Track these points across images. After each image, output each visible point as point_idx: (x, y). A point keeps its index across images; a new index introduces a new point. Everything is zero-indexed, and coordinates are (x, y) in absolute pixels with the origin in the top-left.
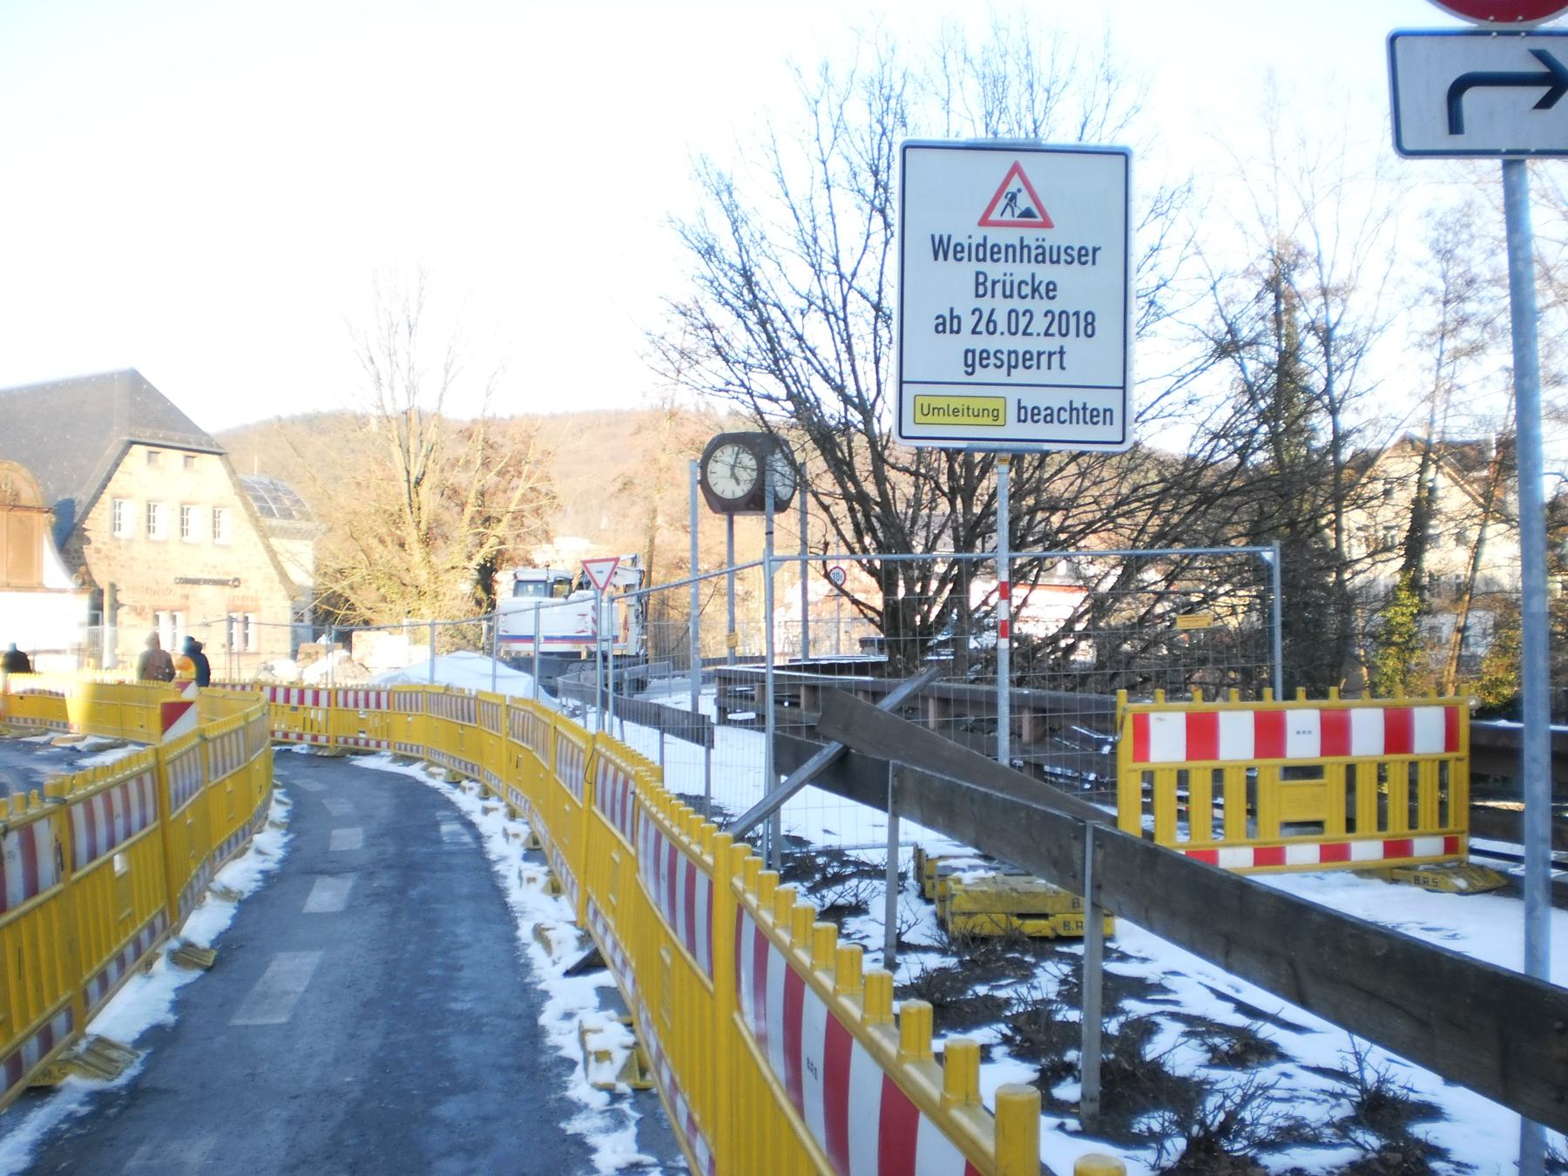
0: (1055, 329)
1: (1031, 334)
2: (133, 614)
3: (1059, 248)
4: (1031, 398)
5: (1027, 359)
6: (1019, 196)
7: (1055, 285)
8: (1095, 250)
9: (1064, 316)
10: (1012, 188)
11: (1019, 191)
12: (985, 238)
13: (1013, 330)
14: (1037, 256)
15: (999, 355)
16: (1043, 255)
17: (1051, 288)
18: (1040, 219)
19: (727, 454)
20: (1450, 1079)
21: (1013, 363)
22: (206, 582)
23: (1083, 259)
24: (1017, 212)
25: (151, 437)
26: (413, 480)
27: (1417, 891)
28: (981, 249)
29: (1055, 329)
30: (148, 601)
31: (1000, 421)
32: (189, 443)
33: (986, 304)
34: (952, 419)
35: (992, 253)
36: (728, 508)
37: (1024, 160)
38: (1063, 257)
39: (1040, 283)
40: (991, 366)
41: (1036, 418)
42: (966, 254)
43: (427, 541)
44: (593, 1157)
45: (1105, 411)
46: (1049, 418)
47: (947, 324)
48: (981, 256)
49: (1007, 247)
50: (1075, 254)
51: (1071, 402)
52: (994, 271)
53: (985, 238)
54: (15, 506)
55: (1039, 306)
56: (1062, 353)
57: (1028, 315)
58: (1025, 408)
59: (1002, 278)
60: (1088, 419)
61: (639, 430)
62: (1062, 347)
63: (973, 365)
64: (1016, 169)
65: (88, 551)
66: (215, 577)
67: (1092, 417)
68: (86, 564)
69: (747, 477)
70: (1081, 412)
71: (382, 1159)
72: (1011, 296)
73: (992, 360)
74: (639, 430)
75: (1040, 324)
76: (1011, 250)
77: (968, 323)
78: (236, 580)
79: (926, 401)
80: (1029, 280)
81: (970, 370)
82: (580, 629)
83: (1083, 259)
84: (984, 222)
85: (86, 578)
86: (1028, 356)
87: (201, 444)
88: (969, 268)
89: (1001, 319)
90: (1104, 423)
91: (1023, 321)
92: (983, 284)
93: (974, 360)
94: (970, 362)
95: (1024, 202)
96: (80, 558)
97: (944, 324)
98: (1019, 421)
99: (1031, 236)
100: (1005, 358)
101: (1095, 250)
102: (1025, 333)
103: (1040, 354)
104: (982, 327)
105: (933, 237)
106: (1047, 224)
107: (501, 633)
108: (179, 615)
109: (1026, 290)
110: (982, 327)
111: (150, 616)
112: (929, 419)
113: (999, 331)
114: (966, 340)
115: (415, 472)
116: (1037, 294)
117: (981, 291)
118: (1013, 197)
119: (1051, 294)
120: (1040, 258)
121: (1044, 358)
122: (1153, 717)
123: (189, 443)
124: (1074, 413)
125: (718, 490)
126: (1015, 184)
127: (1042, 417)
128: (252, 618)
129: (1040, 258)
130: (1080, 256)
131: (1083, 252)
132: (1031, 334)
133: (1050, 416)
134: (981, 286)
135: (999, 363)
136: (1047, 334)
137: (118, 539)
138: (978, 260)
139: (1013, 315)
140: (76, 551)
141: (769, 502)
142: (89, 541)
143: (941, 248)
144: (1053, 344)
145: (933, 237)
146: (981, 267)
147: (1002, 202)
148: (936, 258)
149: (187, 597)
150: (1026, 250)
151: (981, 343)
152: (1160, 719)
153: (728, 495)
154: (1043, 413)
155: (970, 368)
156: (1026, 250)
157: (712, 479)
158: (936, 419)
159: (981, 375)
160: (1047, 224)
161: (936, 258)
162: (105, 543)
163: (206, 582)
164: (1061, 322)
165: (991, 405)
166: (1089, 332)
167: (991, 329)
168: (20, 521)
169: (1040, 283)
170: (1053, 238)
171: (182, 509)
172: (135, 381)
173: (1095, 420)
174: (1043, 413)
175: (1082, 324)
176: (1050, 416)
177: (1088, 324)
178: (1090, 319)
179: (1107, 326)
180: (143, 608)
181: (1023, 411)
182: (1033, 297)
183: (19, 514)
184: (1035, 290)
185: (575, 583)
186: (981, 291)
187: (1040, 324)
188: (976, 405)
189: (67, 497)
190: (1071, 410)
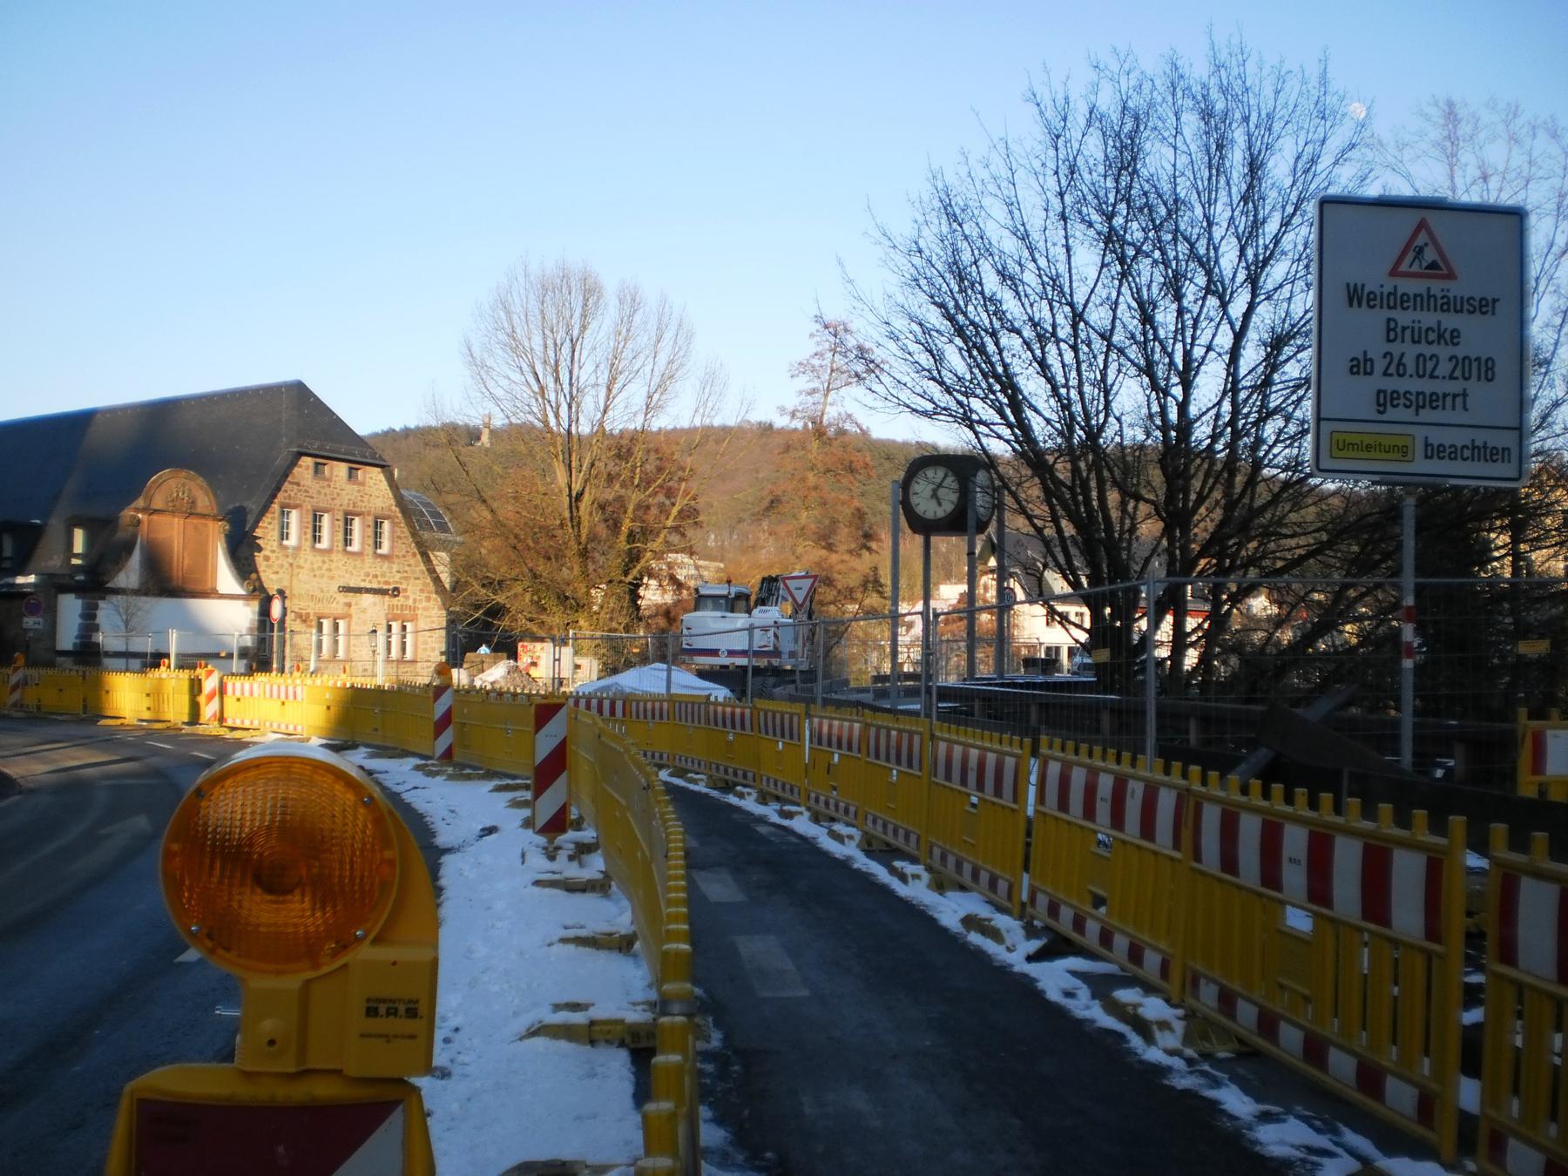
0: (1458, 373)
1: (1437, 377)
2: (298, 621)
4: (1438, 437)
5: (1434, 401)
6: (1427, 250)
7: (1459, 333)
8: (1495, 301)
9: (1467, 362)
10: (1420, 241)
11: (1426, 244)
13: (1421, 373)
14: (1443, 304)
16: (1448, 305)
17: (1455, 336)
18: (1445, 271)
19: (936, 474)
21: (1421, 404)
22: (368, 591)
23: (1484, 309)
24: (1425, 264)
25: (319, 448)
26: (574, 494)
27: (606, 952)
29: (1458, 373)
30: (312, 609)
31: (1409, 457)
32: (354, 455)
33: (1396, 348)
34: (1365, 455)
36: (925, 527)
37: (1432, 218)
38: (1466, 307)
39: (1446, 330)
40: (1401, 407)
41: (1441, 455)
42: (1378, 302)
43: (584, 554)
45: (1503, 449)
46: (1453, 455)
47: (1360, 366)
48: (1392, 304)
49: (1415, 296)
50: (1476, 304)
51: (1365, 353)
52: (1404, 318)
54: (191, 514)
55: (1444, 352)
56: (1465, 395)
57: (1434, 359)
58: (1432, 445)
59: (1411, 325)
60: (1488, 457)
61: (788, 448)
62: (1465, 390)
63: (1384, 405)
64: (1422, 225)
65: (259, 558)
66: (375, 586)
67: (1492, 455)
68: (257, 572)
69: (949, 499)
70: (1482, 450)
72: (1419, 342)
73: (1402, 401)
74: (788, 448)
75: (1444, 368)
77: (1380, 365)
78: (396, 589)
79: (1342, 437)
80: (1435, 327)
81: (1382, 409)
82: (763, 644)
84: (1394, 272)
85: (257, 584)
86: (1434, 398)
87: (366, 457)
88: (1380, 315)
89: (1409, 361)
90: (1503, 461)
91: (1430, 365)
92: (1394, 330)
93: (1385, 400)
95: (1430, 255)
96: (250, 565)
97: (1358, 366)
98: (1426, 457)
99: (1436, 287)
100: (1413, 398)
101: (1495, 301)
102: (1432, 376)
103: (1445, 395)
104: (1392, 370)
105: (1348, 285)
106: (1451, 276)
107: (685, 646)
108: (341, 623)
109: (1432, 336)
110: (1392, 370)
111: (314, 623)
112: (1344, 454)
113: (1408, 374)
114: (1378, 381)
115: (576, 487)
116: (1442, 341)
117: (1392, 337)
118: (1420, 251)
121: (1449, 399)
122: (1549, 733)
123: (354, 455)
124: (1476, 451)
125: (920, 510)
126: (1422, 239)
127: (1446, 454)
128: (409, 626)
130: (1481, 306)
131: (1484, 303)
132: (1437, 377)
133: (1454, 453)
134: (1392, 332)
135: (1408, 403)
136: (1451, 377)
137: (286, 548)
139: (1421, 359)
140: (246, 559)
141: (971, 522)
142: (260, 549)
143: (1355, 296)
144: (1455, 387)
145: (1348, 285)
146: (1393, 314)
147: (1411, 255)
148: (1351, 305)
149: (349, 605)
150: (1432, 299)
151: (1391, 384)
152: (1556, 736)
153: (930, 515)
154: (1448, 451)
155: (1381, 407)
156: (1432, 299)
157: (914, 500)
158: (1351, 454)
159: (1391, 414)
160: (1451, 276)
161: (1351, 305)
162: (273, 551)
163: (368, 591)
164: (1465, 367)
165: (1400, 442)
166: (1490, 376)
167: (1401, 372)
168: (196, 528)
169: (1446, 330)
170: (1457, 289)
171: (346, 519)
172: (299, 392)
173: (1495, 458)
174: (1448, 451)
175: (1483, 369)
176: (1454, 453)
177: (1487, 370)
178: (1490, 363)
179: (1503, 369)
180: (308, 615)
181: (1429, 448)
182: (1439, 343)
183: (195, 521)
184: (1440, 336)
185: (753, 598)
186: (1392, 337)
187: (1444, 368)
188: (1387, 442)
189: (237, 505)
190: (1474, 448)
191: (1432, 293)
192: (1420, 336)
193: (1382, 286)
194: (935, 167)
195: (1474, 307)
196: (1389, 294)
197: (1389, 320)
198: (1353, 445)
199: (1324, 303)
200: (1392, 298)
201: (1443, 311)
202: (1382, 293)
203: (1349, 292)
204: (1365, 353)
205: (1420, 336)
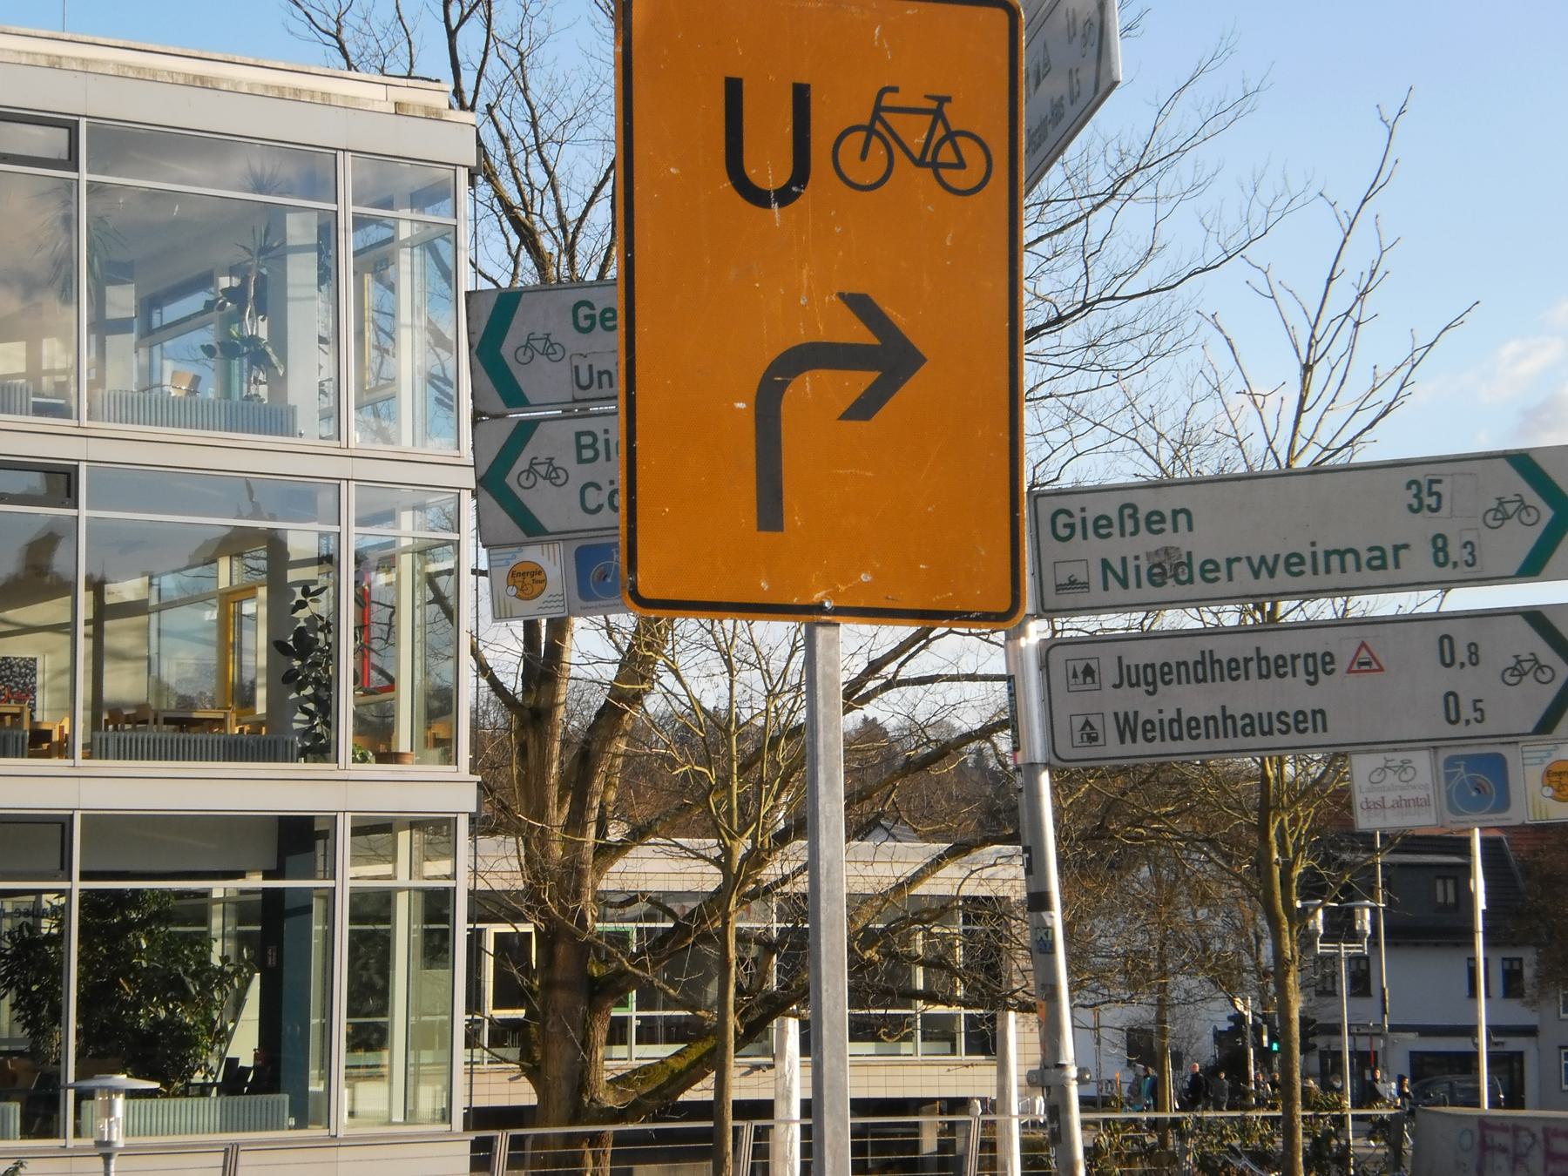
3: (1270, 714)
12: (1179, 711)
14: (1244, 727)
15: (1284, 728)
20: (637, 1001)
23: (1301, 726)
28: (1200, 667)
35: (1190, 729)
38: (1277, 725)
42: (1157, 734)
44: (240, 1064)
49: (1207, 719)
50: (1291, 720)
51: (1223, 708)
53: (1179, 711)
71: (1144, 913)
76: (1211, 723)
83: (1301, 726)
90: (1179, 682)
94: (1311, 669)
119: (1329, 668)
120: (1248, 730)
129: (1248, 730)
130: (1297, 722)
138: (1173, 738)
156: (1229, 722)
191: (1228, 713)
192: (1138, 678)
193: (1313, 544)
194: (1124, 149)
195: (1287, 724)
196: (1172, 721)
197: (579, 435)
198: (1342, 554)
199: (1006, 229)
200: (1175, 725)
201: (1246, 735)
202: (1161, 721)
203: (1118, 726)
204: (1223, 708)
205: (1138, 678)
